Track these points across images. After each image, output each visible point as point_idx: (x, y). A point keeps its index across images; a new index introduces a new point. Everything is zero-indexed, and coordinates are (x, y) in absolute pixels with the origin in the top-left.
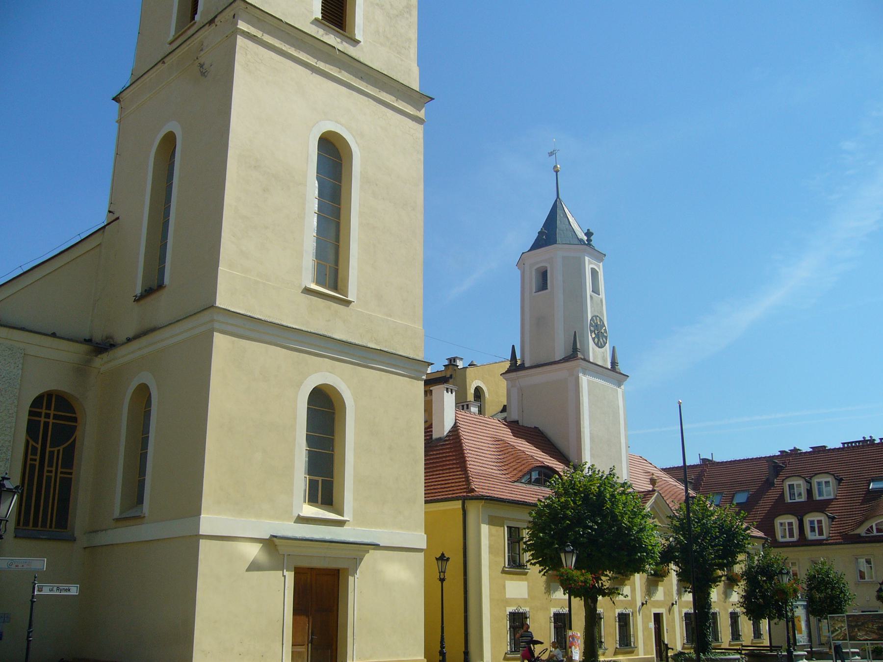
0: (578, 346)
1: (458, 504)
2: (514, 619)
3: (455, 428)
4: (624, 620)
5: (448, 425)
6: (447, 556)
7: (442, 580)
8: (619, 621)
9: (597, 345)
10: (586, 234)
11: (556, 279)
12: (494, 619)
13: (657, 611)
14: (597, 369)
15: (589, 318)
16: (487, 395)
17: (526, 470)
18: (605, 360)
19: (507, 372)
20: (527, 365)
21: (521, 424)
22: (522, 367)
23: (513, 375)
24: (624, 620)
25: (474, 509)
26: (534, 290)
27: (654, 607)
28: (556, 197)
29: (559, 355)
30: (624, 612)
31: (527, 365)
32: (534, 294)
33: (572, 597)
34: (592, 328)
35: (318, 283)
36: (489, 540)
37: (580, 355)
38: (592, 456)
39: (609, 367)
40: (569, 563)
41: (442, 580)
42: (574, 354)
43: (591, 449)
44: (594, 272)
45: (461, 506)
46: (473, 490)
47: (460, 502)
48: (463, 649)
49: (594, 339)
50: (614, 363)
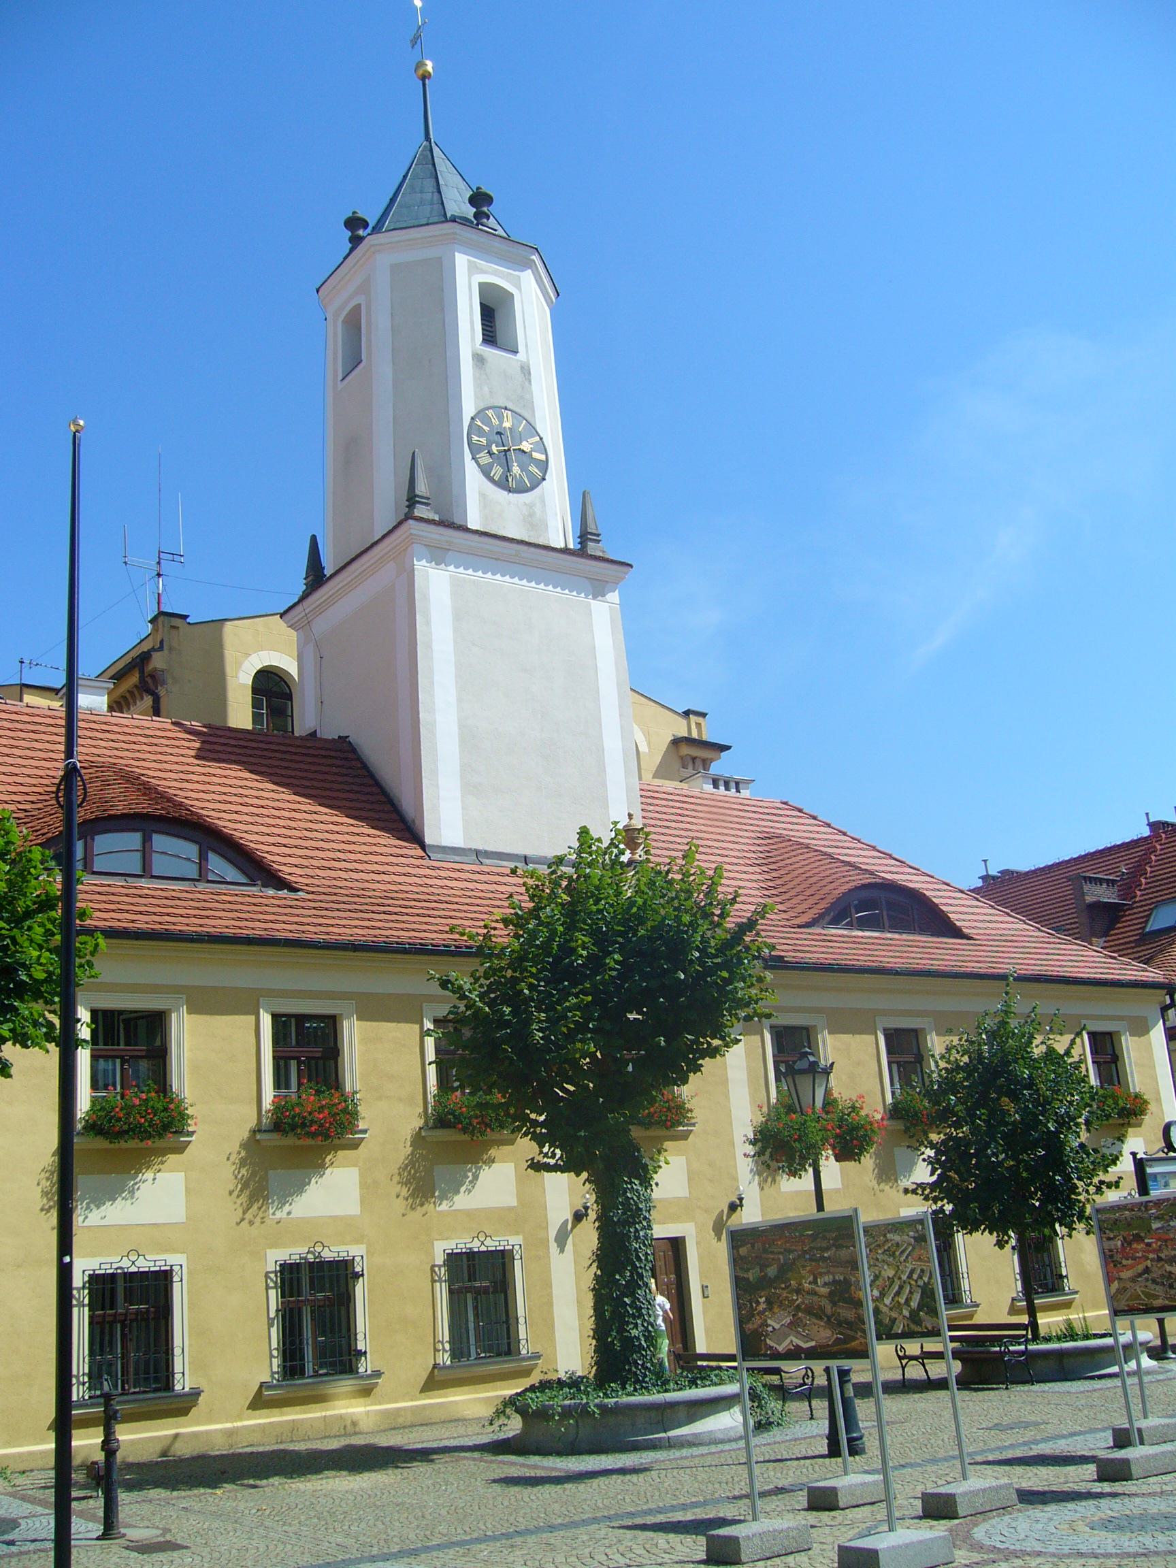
0: (421, 488)
9: (503, 484)
50: (585, 536)
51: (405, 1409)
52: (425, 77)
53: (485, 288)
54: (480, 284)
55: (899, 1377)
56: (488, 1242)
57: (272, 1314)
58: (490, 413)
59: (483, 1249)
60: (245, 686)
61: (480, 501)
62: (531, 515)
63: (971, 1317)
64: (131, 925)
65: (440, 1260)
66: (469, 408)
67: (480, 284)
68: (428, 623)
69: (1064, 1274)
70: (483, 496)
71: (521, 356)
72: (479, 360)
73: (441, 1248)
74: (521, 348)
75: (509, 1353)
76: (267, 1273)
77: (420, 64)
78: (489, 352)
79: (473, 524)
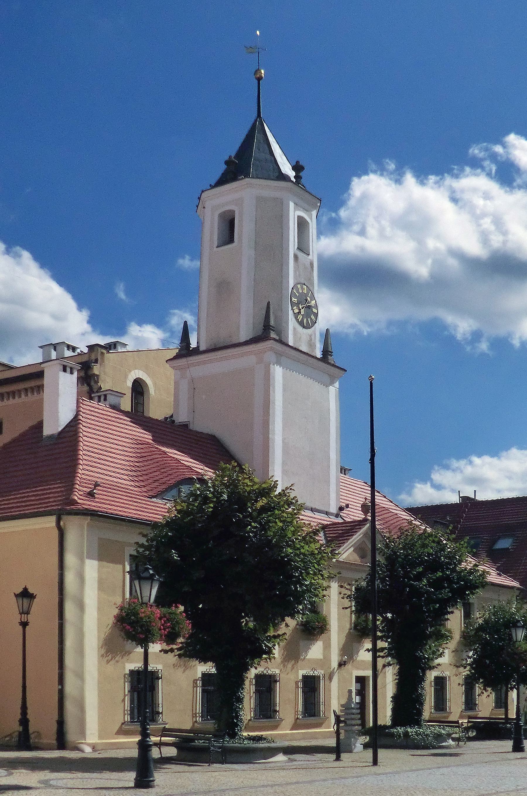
0: (272, 323)
1: (50, 522)
2: (139, 681)
3: (73, 425)
4: (310, 686)
5: (65, 416)
6: (31, 591)
7: (24, 624)
8: (256, 685)
9: (301, 323)
10: (294, 168)
11: (244, 229)
12: (103, 680)
13: (361, 673)
14: (298, 356)
15: (291, 284)
16: (152, 390)
17: (172, 481)
18: (311, 345)
19: (177, 357)
20: (202, 348)
21: (191, 427)
22: (197, 351)
23: (183, 362)
24: (310, 686)
25: (76, 531)
26: (216, 244)
27: (358, 668)
28: (255, 114)
29: (244, 335)
30: (311, 673)
31: (202, 348)
32: (215, 249)
33: (478, 688)
34: (295, 300)
35: (104, 333)
36: (99, 571)
37: (273, 335)
38: (285, 472)
39: (319, 355)
40: (146, 593)
41: (24, 624)
42: (267, 331)
43: (284, 463)
44: (302, 224)
45: (54, 524)
46: (75, 503)
47: (53, 518)
48: (56, 717)
49: (296, 315)
50: (326, 352)
51: (288, 734)
52: (259, 79)
53: (299, 217)
54: (298, 216)
55: (160, 756)
56: (269, 672)
57: (126, 693)
58: (299, 286)
59: (314, 675)
60: (128, 387)
61: (294, 332)
62: (311, 340)
63: (448, 717)
64: (89, 507)
65: (300, 677)
66: (291, 284)
67: (298, 216)
68: (274, 392)
69: (278, 709)
70: (295, 329)
71: (310, 257)
72: (296, 257)
73: (302, 673)
74: (311, 253)
75: (314, 715)
76: (125, 674)
77: (258, 71)
78: (300, 255)
79: (291, 344)
